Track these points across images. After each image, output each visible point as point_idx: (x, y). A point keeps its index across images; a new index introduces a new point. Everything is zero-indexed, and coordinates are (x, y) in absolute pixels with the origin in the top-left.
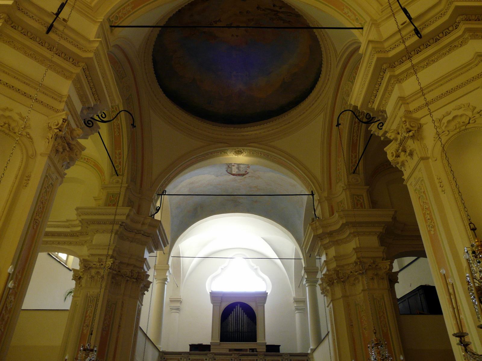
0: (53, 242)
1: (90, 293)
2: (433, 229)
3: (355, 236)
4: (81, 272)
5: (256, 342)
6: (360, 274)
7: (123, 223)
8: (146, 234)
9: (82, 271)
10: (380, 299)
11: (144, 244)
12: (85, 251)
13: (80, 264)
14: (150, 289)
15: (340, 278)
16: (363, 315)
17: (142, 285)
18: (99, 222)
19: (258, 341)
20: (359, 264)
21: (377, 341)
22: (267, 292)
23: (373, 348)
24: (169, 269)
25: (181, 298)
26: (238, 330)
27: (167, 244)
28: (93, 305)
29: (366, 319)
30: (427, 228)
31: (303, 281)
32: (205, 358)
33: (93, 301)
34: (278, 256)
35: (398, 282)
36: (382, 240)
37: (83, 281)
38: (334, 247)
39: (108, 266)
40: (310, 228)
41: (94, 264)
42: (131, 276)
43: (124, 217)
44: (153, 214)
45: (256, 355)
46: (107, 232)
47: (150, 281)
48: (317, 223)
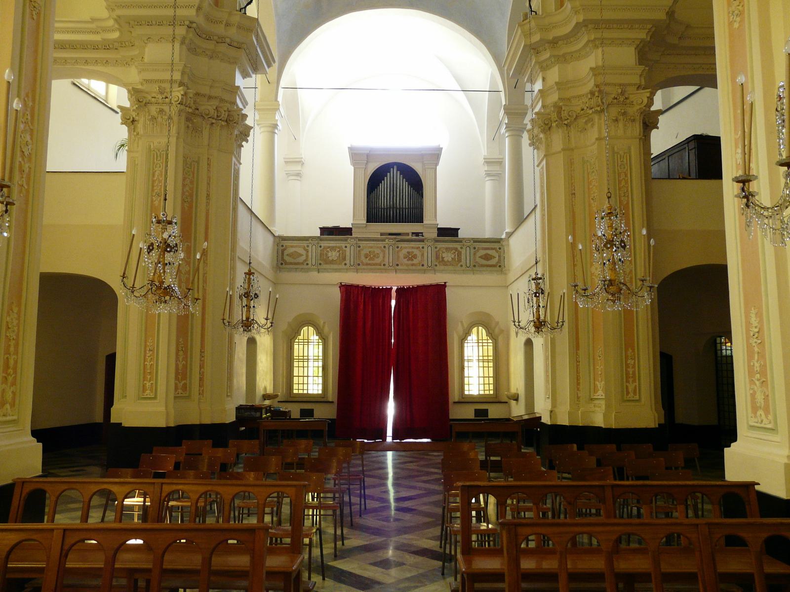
0: (76, 61)
1: (153, 144)
2: (738, 19)
3: (596, 47)
4: (133, 110)
5: (423, 222)
6: (596, 112)
7: (191, 22)
8: (235, 44)
9: (135, 108)
10: (624, 153)
11: (234, 62)
12: (134, 75)
13: (130, 97)
14: (250, 139)
15: (563, 118)
16: (592, 178)
17: (236, 132)
18: (149, 22)
19: (425, 222)
20: (597, 94)
21: (611, 209)
22: (441, 147)
23: (602, 218)
24: (279, 109)
25: (302, 158)
26: (395, 206)
27: (272, 63)
28: (162, 163)
29: (596, 185)
30: (729, 17)
31: (501, 128)
32: (343, 246)
33: (160, 157)
34: (460, 85)
35: (658, 128)
36: (642, 56)
37: (140, 126)
38: (557, 65)
39: (175, 99)
40: (520, 31)
41: (153, 97)
42: (217, 116)
43: (192, 12)
44: (242, 6)
45: (423, 241)
46: (167, 40)
47: (250, 125)
48: (533, 23)
